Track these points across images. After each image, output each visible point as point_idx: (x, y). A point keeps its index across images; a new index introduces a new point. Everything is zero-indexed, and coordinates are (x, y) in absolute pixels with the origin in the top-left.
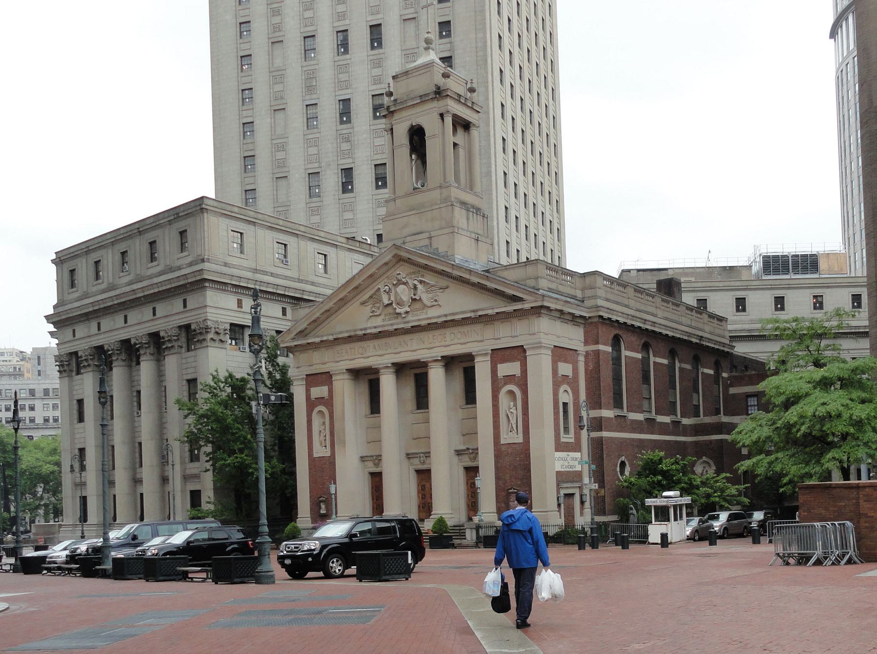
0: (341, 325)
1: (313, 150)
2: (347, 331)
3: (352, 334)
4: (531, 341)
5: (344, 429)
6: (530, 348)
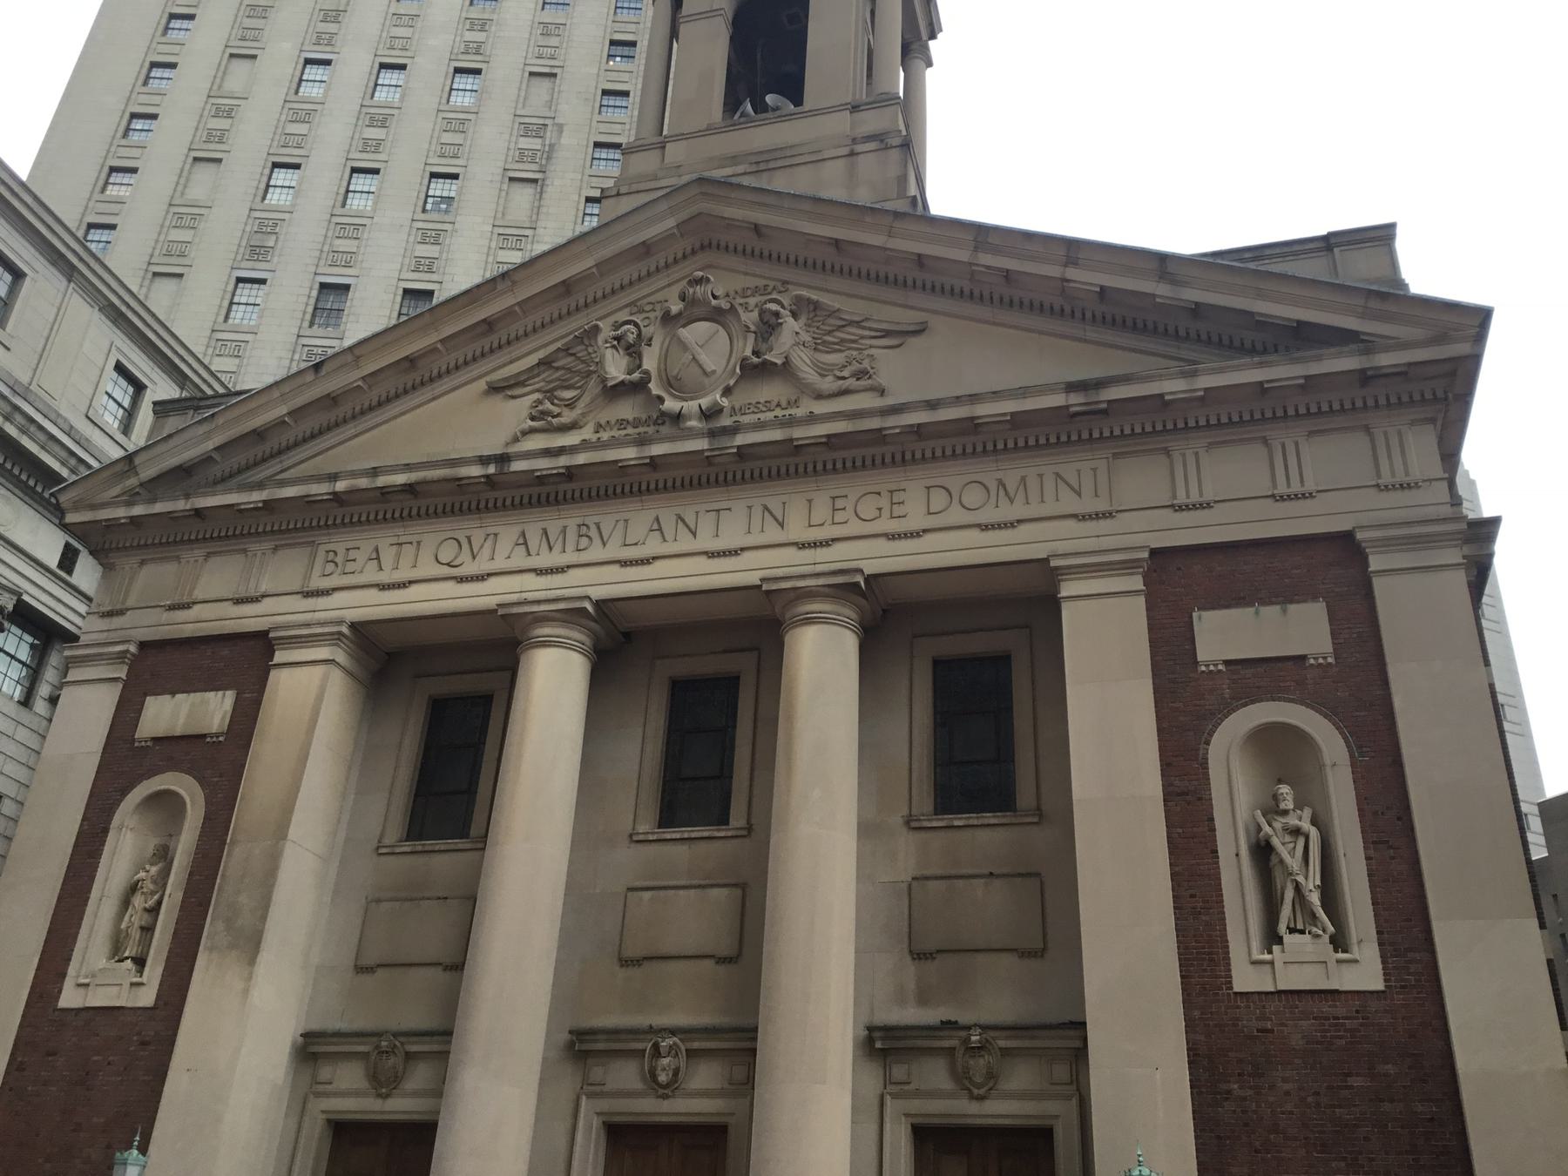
2: (408, 467)
6: (1387, 544)
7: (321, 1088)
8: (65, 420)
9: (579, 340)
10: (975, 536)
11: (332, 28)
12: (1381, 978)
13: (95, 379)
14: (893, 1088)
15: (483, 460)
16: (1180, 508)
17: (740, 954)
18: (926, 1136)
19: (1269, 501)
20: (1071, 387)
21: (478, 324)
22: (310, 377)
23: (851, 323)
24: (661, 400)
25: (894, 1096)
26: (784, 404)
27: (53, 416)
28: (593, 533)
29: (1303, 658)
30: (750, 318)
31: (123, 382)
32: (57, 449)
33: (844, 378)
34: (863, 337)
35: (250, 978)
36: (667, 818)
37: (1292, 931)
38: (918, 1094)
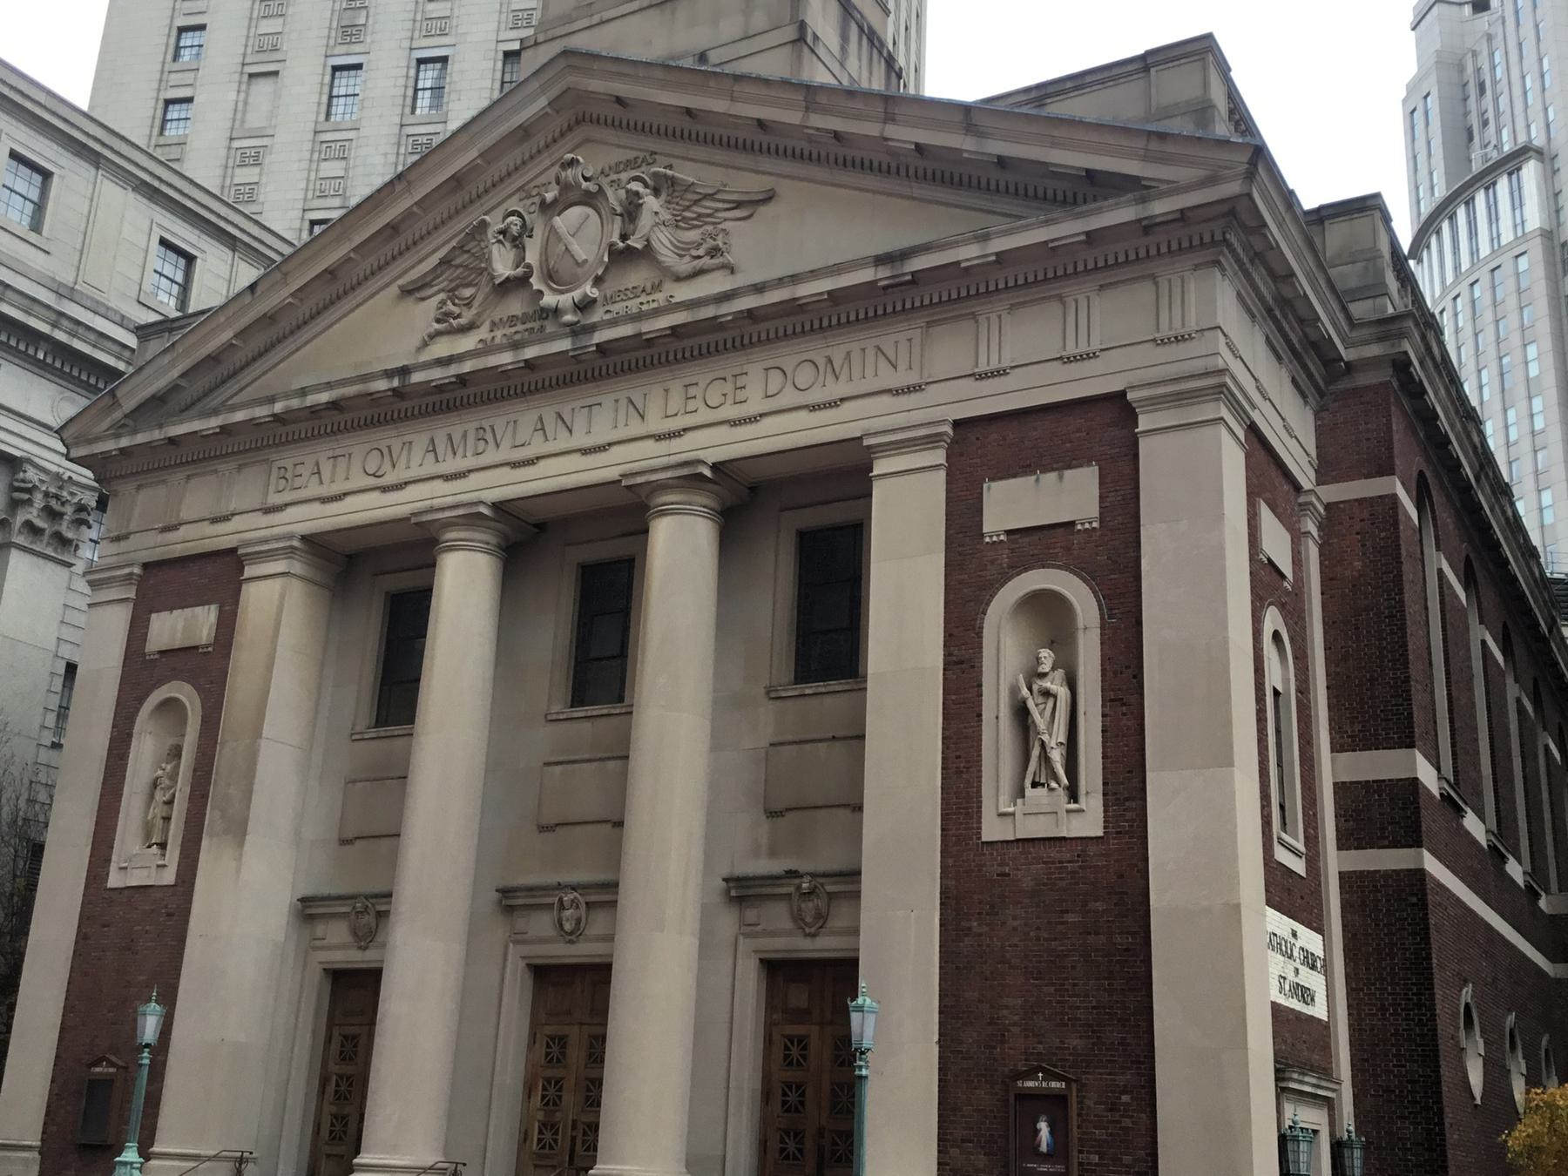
1: (333, 169)
2: (329, 386)
5: (249, 774)
6: (1155, 403)
7: (318, 943)
8: (116, 312)
12: (1101, 824)
13: (140, 261)
14: (748, 929)
15: (388, 374)
16: (981, 377)
18: (776, 970)
19: (1057, 364)
20: (880, 260)
21: (379, 232)
22: (248, 298)
23: (706, 196)
24: (541, 293)
26: (648, 289)
27: (102, 310)
28: (489, 436)
29: (1072, 523)
30: (614, 198)
31: (172, 256)
32: (109, 345)
33: (699, 257)
34: (717, 210)
36: (578, 700)
37: (1035, 785)
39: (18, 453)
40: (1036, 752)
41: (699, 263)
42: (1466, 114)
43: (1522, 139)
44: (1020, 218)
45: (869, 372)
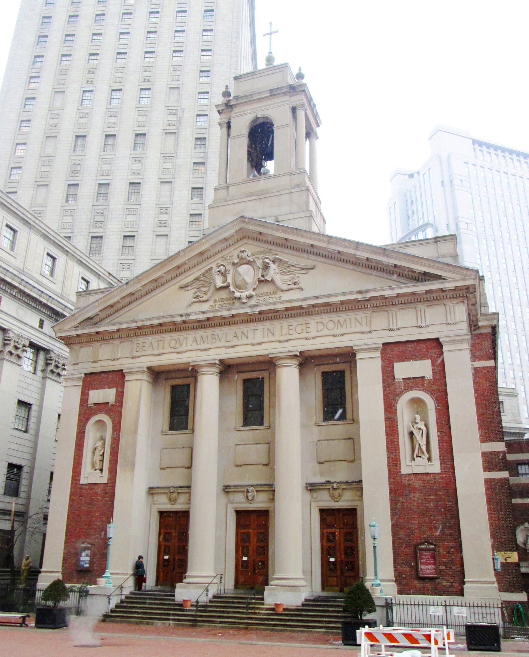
0: (147, 312)
1: (68, 219)
2: (159, 318)
3: (167, 320)
4: (450, 333)
6: (448, 342)
7: (155, 502)
9: (207, 272)
10: (331, 339)
11: (92, 76)
17: (269, 463)
23: (292, 266)
25: (314, 501)
26: (272, 293)
27: (31, 278)
28: (216, 337)
30: (259, 263)
35: (133, 474)
37: (417, 456)
38: (320, 501)
39: (7, 328)
40: (417, 447)
41: (290, 287)
42: (407, 210)
43: (426, 221)
44: (407, 284)
45: (353, 326)
